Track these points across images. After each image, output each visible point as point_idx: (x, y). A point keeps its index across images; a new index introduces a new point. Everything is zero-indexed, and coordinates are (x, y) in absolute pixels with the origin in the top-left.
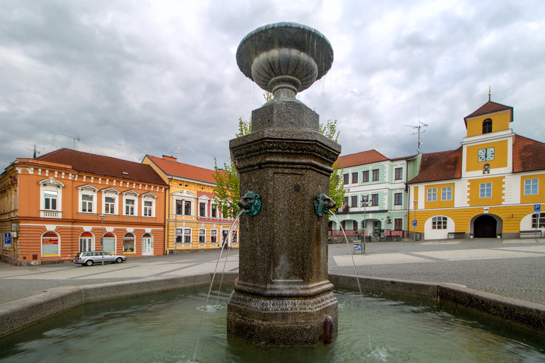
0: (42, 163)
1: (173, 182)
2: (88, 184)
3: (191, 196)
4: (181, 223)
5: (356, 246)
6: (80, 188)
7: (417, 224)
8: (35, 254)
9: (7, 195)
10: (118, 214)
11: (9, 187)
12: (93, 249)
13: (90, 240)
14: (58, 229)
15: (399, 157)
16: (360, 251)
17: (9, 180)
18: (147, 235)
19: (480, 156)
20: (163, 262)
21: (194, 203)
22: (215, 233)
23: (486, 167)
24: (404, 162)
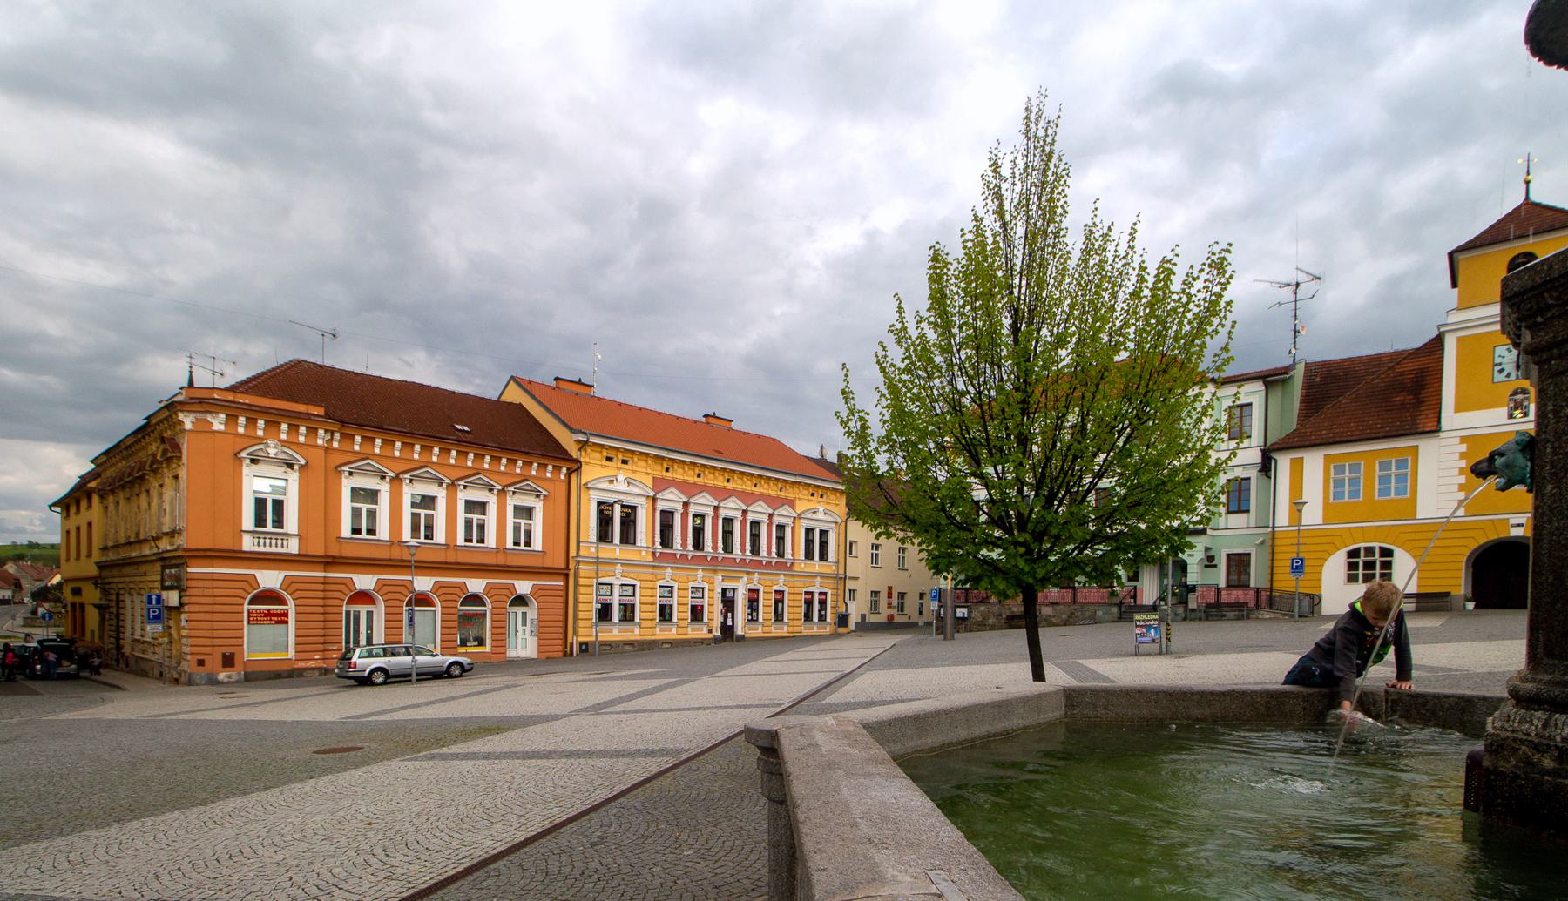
0: (247, 401)
1: (589, 450)
2: (368, 458)
3: (636, 491)
4: (611, 568)
5: (1144, 630)
6: (346, 468)
7: (1306, 569)
8: (228, 651)
9: (148, 491)
10: (444, 542)
11: (155, 466)
12: (379, 637)
13: (370, 614)
14: (288, 583)
15: (1273, 367)
16: (1156, 647)
17: (154, 447)
18: (520, 601)
19: (1500, 364)
20: (579, 676)
21: (644, 511)
22: (700, 594)
23: (1519, 397)
24: (1258, 386)
